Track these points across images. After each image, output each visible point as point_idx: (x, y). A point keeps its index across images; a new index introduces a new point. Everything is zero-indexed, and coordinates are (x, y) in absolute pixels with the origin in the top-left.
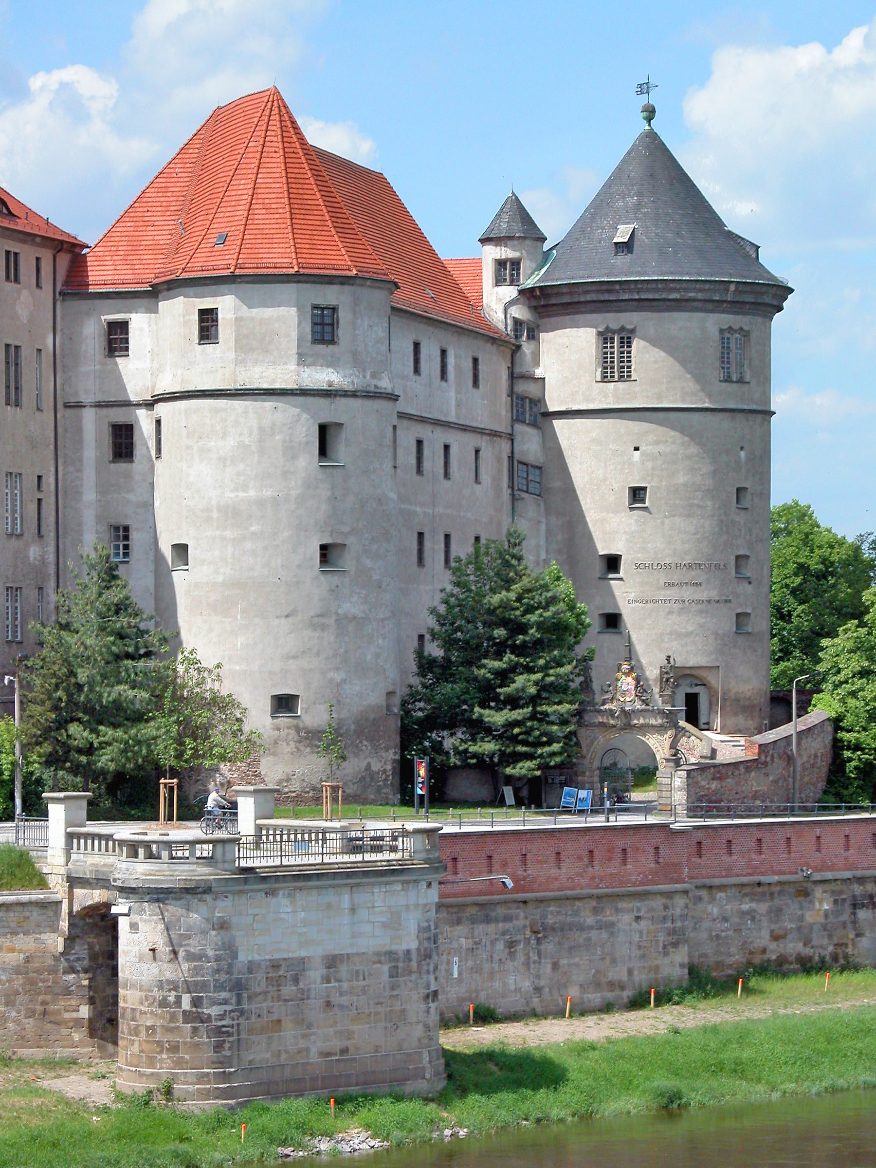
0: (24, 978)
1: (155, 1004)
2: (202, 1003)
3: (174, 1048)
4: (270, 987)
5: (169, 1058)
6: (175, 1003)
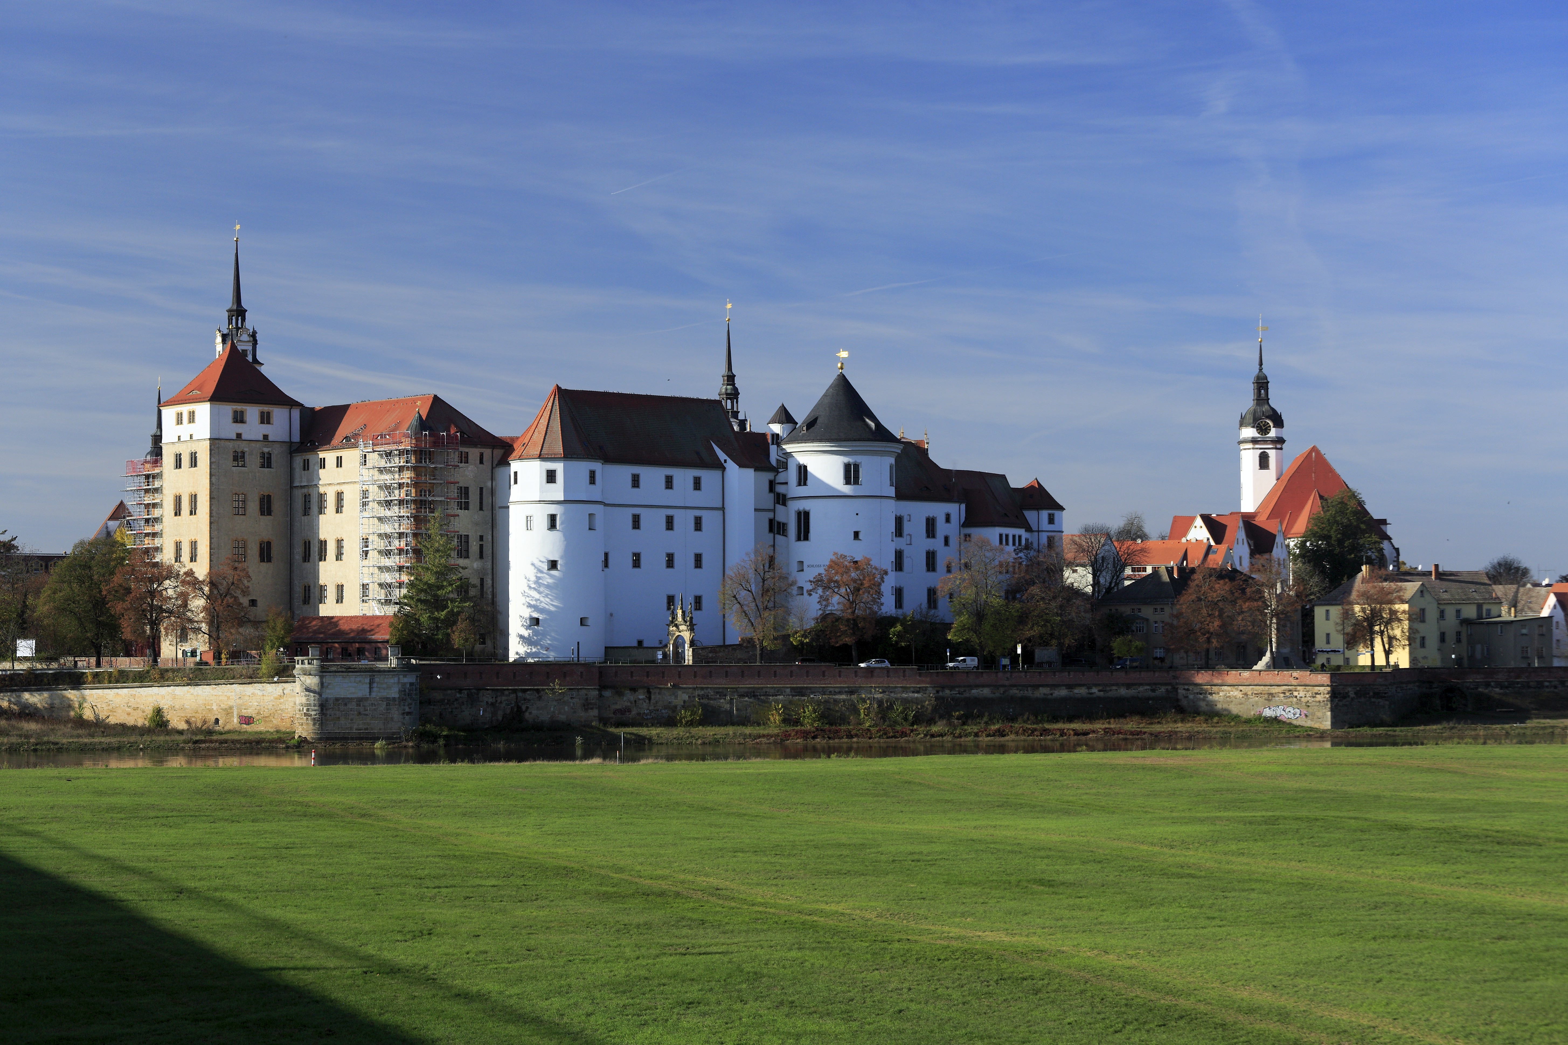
3: (302, 725)
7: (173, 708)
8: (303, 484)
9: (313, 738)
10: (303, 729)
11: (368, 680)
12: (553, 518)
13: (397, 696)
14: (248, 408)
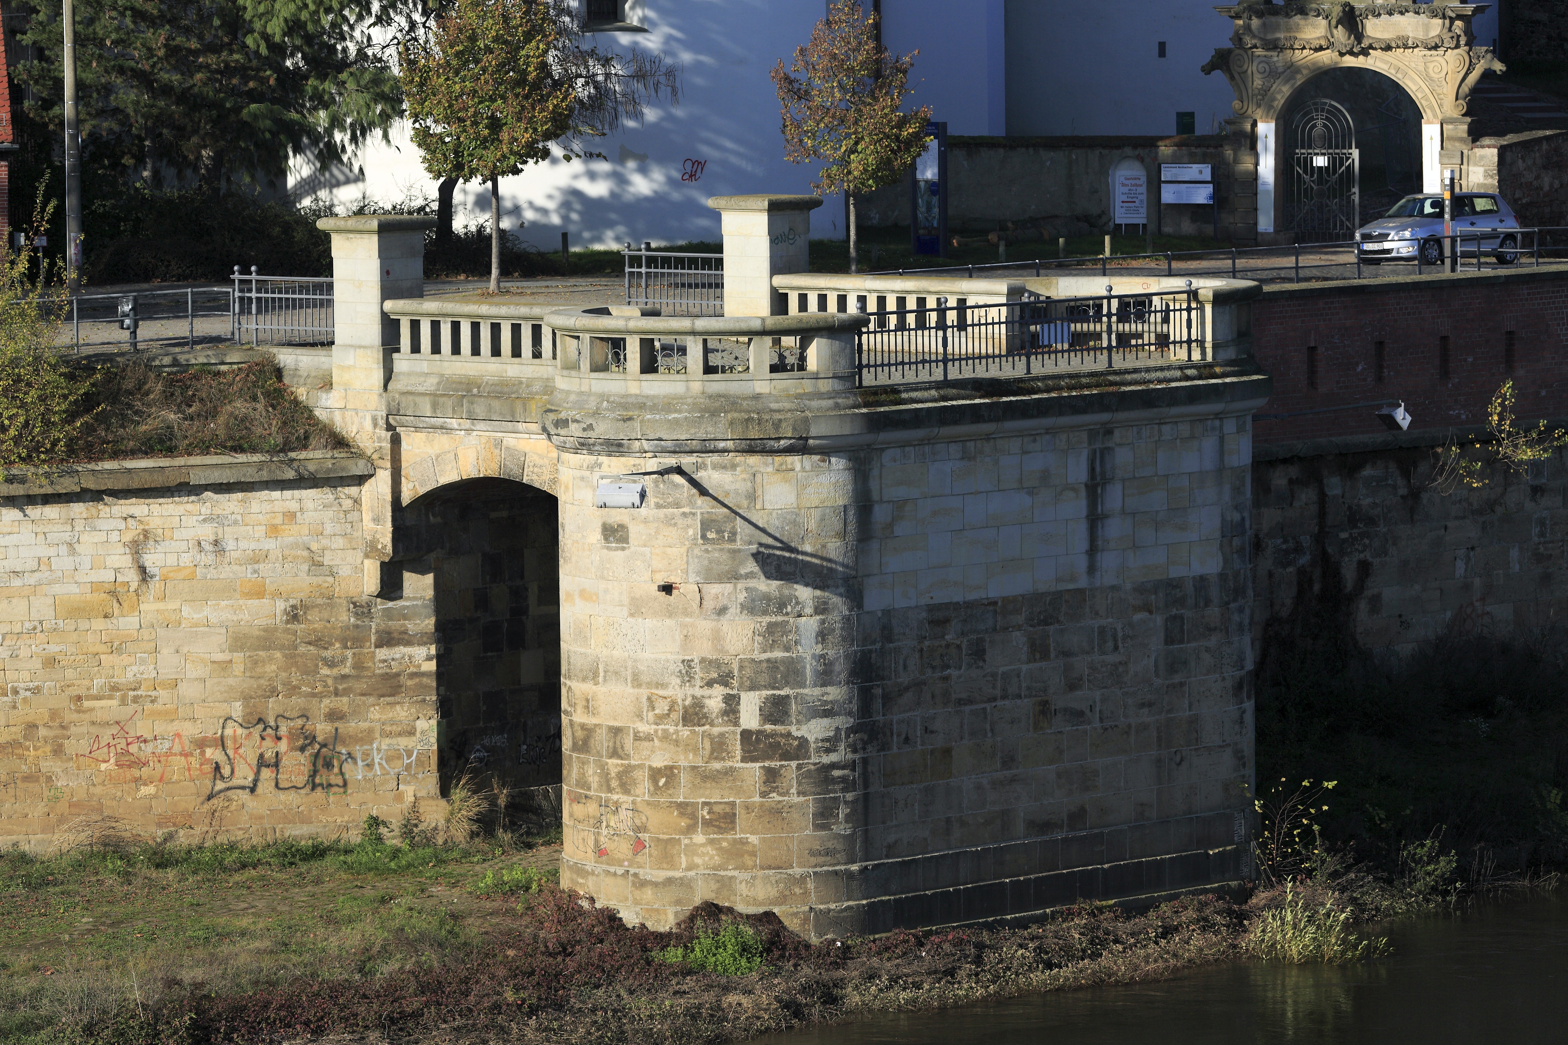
0: (285, 656)
1: (674, 716)
2: (786, 713)
3: (724, 820)
4: (929, 672)
5: (711, 842)
6: (725, 713)
9: (823, 920)
10: (737, 853)
11: (1078, 470)
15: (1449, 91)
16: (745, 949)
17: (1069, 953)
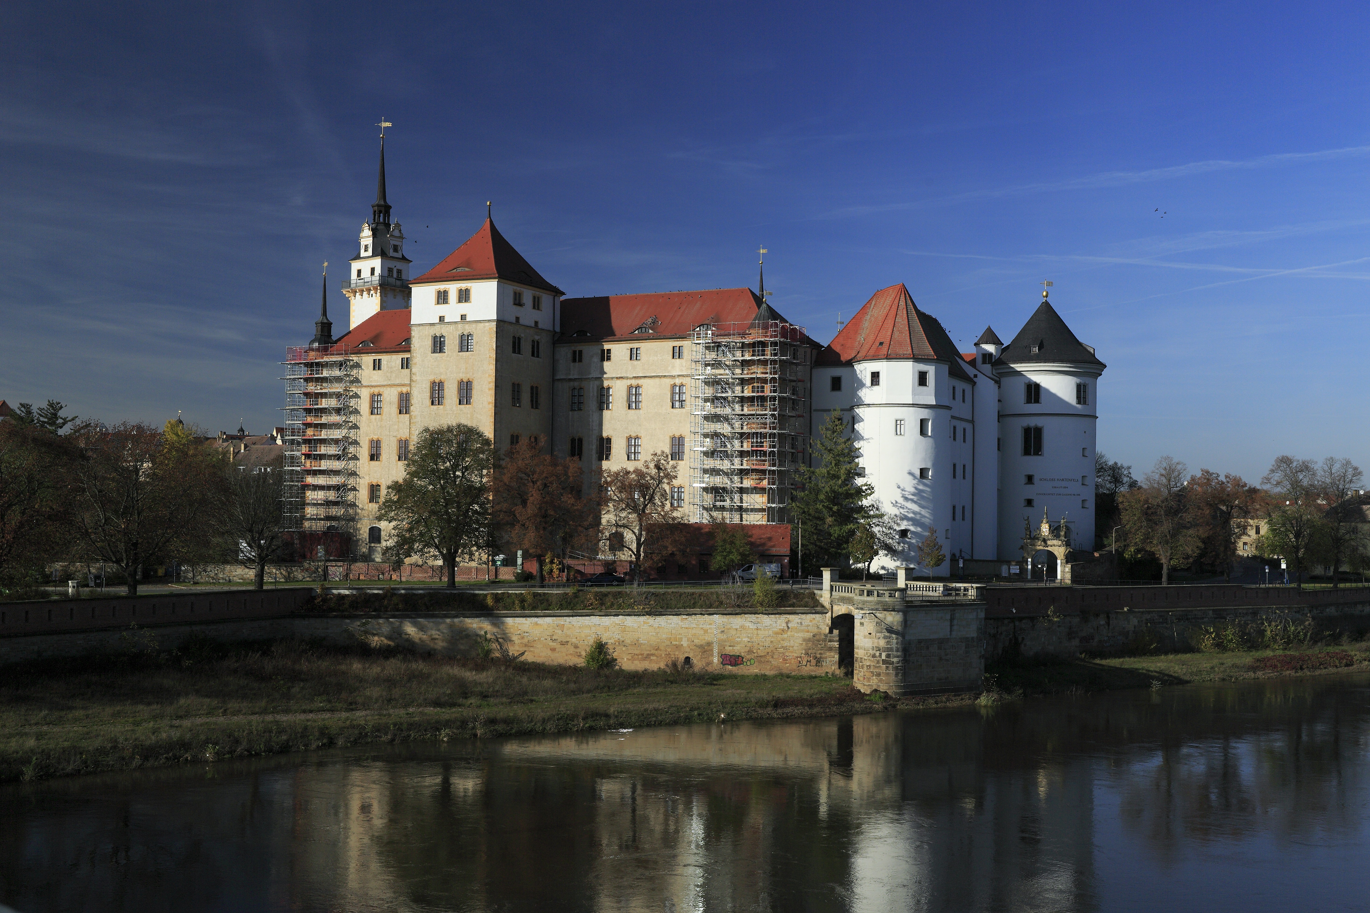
7: (621, 643)
8: (571, 377)
9: (896, 694)
10: (881, 681)
11: (948, 617)
12: (923, 423)
13: (975, 635)
14: (525, 290)
15: (1062, 554)
16: (881, 698)
17: (941, 702)
